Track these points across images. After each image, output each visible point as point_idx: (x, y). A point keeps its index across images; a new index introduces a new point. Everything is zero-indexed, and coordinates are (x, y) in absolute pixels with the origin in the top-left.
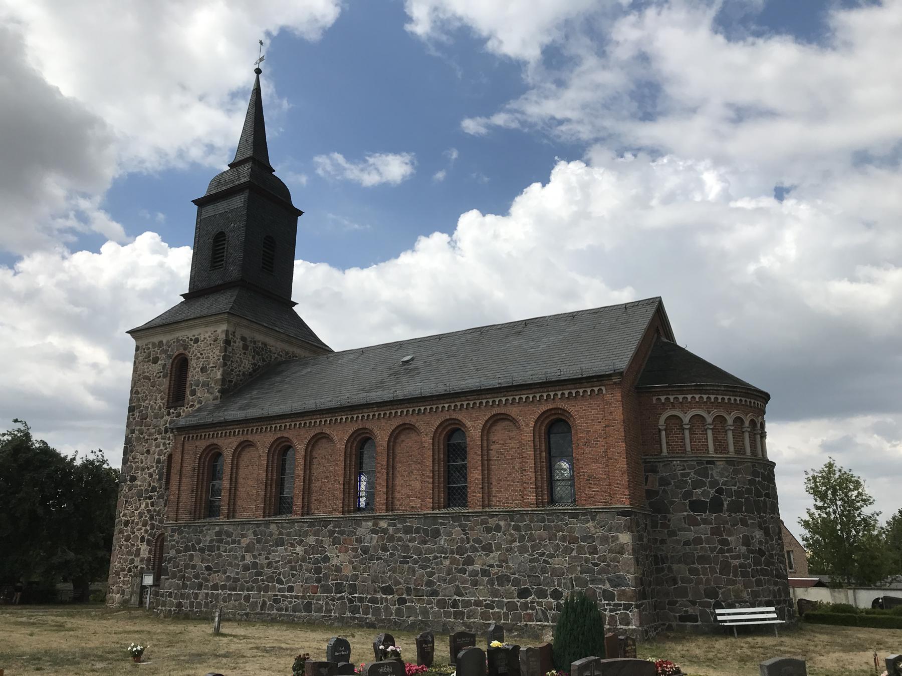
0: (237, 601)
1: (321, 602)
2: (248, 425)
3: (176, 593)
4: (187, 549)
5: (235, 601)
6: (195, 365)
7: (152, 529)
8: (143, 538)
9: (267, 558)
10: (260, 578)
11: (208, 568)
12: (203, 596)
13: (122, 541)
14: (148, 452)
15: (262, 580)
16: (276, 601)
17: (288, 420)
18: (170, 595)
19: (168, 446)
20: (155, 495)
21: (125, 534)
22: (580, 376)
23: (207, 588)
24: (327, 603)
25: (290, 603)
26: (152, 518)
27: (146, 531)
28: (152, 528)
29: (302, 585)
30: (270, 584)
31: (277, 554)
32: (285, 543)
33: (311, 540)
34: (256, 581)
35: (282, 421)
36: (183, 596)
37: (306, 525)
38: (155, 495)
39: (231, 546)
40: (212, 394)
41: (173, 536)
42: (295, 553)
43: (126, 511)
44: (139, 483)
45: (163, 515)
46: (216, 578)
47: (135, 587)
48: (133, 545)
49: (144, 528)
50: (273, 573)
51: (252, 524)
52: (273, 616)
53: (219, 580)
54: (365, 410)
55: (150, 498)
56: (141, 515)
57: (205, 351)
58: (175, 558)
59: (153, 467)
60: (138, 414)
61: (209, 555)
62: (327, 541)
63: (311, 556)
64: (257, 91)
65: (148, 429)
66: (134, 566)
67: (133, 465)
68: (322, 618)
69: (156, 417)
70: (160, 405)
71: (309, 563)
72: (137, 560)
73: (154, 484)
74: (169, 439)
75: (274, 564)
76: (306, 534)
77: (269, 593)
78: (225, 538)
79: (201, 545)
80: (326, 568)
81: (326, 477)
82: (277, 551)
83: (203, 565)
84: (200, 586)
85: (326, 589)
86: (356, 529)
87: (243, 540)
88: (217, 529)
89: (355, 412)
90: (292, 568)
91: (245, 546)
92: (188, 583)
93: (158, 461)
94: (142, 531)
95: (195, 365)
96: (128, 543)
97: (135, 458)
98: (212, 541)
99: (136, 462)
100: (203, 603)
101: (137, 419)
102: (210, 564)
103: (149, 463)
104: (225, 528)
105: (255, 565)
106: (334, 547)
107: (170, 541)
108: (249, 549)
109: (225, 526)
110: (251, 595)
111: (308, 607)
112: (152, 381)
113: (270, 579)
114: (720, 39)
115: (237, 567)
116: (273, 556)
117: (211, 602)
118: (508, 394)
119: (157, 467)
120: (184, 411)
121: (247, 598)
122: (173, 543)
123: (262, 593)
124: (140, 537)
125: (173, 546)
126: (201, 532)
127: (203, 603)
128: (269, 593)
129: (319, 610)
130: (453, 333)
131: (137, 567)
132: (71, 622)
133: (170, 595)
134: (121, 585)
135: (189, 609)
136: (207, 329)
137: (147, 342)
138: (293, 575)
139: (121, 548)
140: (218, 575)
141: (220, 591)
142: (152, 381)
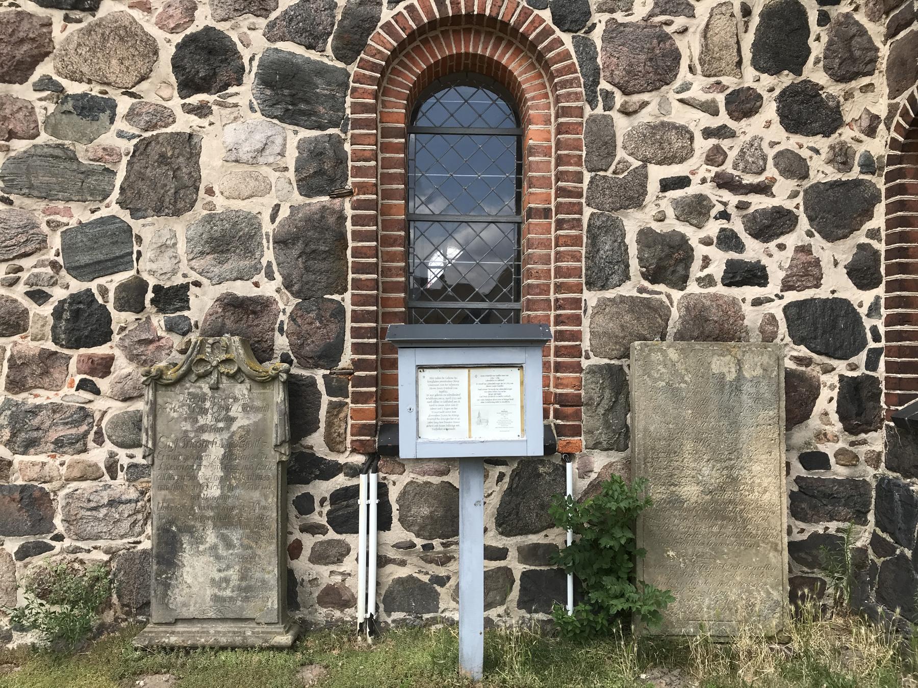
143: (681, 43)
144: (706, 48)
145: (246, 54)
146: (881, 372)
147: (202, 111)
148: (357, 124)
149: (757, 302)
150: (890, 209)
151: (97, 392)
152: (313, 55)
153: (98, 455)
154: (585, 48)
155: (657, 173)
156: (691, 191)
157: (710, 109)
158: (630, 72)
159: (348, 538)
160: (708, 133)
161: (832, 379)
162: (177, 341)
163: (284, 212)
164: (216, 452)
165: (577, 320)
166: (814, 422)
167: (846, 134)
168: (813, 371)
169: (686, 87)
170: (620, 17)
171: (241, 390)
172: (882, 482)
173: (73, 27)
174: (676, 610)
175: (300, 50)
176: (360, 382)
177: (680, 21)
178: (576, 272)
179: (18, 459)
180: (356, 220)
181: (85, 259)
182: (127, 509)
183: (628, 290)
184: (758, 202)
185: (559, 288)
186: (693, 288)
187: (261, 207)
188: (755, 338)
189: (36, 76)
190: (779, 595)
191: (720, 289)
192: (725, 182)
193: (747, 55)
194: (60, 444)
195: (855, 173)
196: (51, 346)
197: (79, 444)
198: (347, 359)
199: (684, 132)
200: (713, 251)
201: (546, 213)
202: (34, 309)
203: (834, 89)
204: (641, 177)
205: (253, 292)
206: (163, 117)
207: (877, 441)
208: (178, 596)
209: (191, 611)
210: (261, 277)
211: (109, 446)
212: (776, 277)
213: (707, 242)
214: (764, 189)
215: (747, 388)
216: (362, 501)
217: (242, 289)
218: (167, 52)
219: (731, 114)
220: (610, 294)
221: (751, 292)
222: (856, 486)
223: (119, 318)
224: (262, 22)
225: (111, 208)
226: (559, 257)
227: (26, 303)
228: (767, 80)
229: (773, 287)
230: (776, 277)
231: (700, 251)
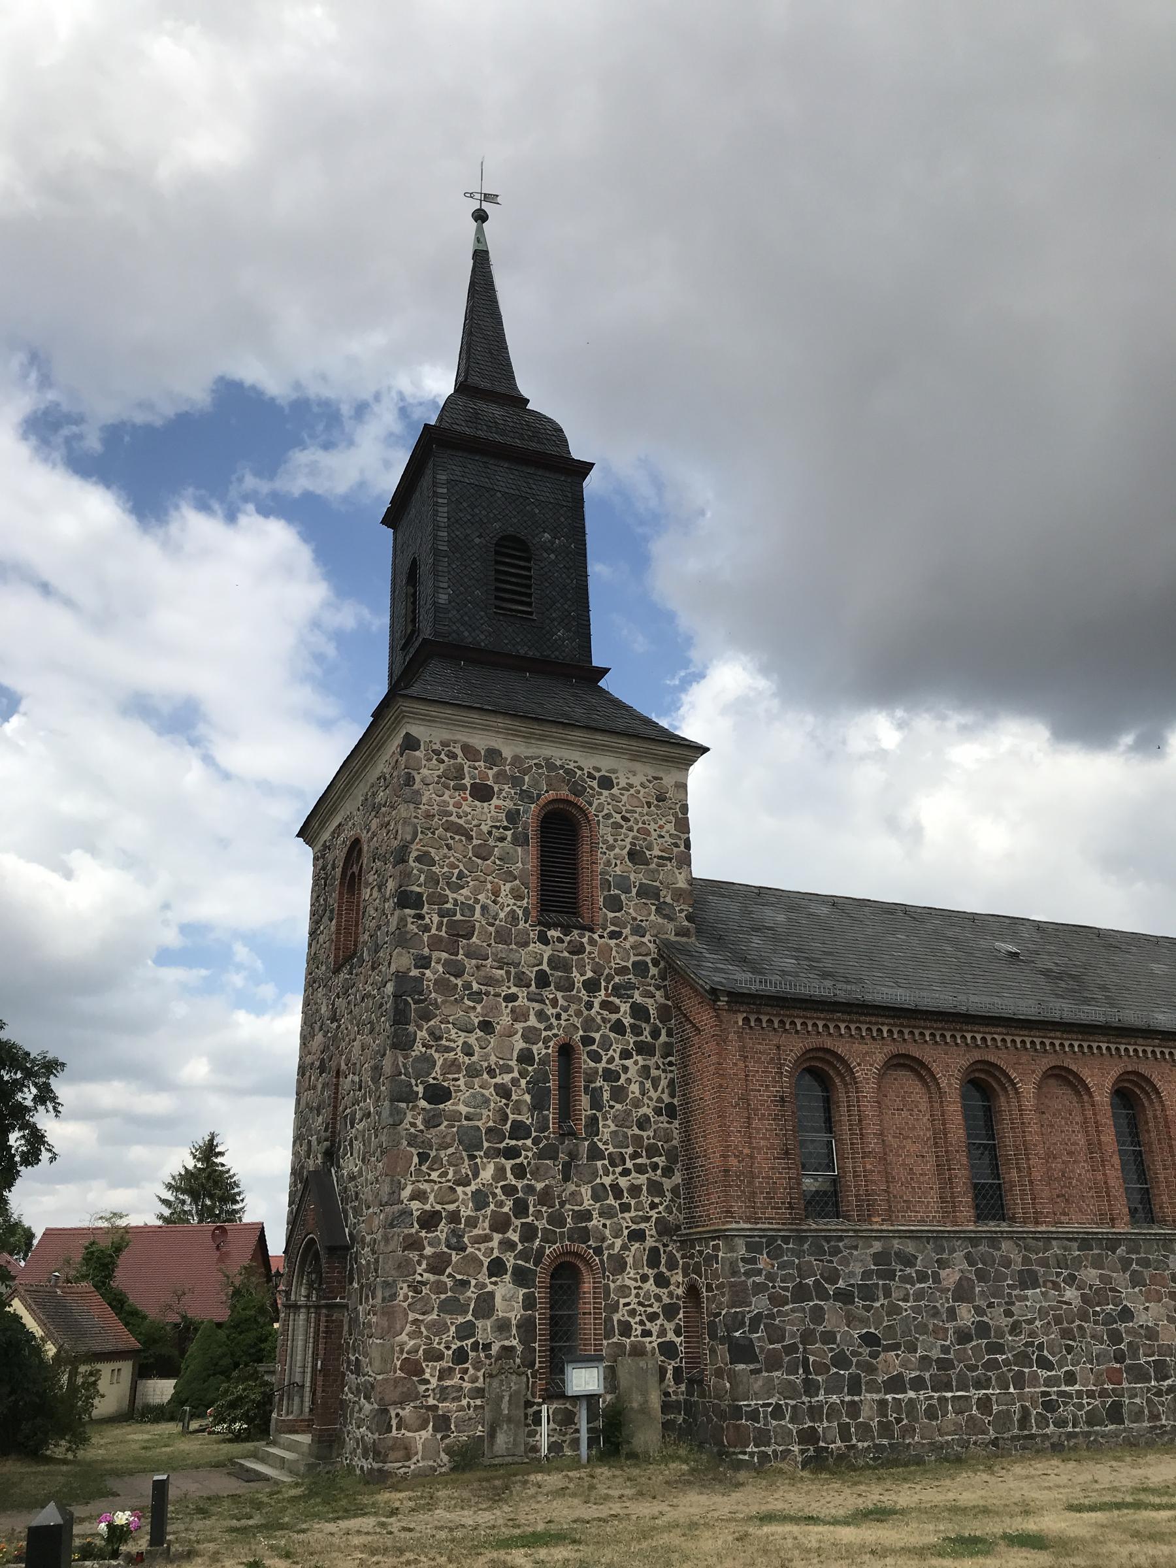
0: (962, 1413)
1: (1137, 1400)
2: (913, 1022)
3: (794, 1407)
4: (801, 1293)
5: (957, 1414)
6: (611, 839)
9: (1008, 1313)
10: (1001, 1357)
12: (871, 1408)
15: (1007, 1362)
16: (1049, 1406)
17: (999, 1030)
18: (778, 1412)
19: (553, 1020)
20: (528, 1149)
21: (428, 1251)
22: (1058, 1020)
23: (873, 1387)
24: (1149, 1401)
25: (1080, 1407)
26: (521, 1208)
27: (508, 1245)
28: (529, 1233)
29: (1091, 1369)
30: (1026, 1370)
31: (1028, 1304)
32: (1041, 1281)
33: (1091, 1275)
34: (992, 1365)
35: (987, 1030)
36: (815, 1412)
37: (1075, 1245)
38: (528, 1149)
39: (918, 1286)
40: (671, 919)
41: (753, 1261)
42: (1066, 1303)
43: (426, 1186)
44: (464, 1110)
45: (562, 1204)
46: (892, 1362)
47: (505, 1405)
48: (465, 1284)
49: (497, 1237)
50: (1027, 1345)
51: (960, 1238)
52: (1055, 1440)
53: (902, 1366)
54: (1140, 1041)
55: (511, 1153)
56: (480, 1200)
57: (636, 815)
58: (772, 1316)
59: (509, 1070)
60: (436, 919)
61: (868, 1309)
62: (1120, 1279)
63: (1098, 1309)
64: (481, 258)
65: (478, 967)
66: (476, 1343)
67: (436, 1056)
68: (1150, 1432)
69: (502, 937)
70: (513, 911)
71: (1096, 1322)
72: (485, 1330)
73: (519, 1118)
74: (554, 1003)
75: (1024, 1325)
76: (1078, 1263)
77: (1027, 1390)
78: (899, 1267)
79: (841, 1284)
80: (1128, 1331)
81: (1070, 1153)
82: (1026, 1298)
83: (855, 1334)
84: (855, 1386)
85: (1139, 1374)
86: (1166, 1257)
87: (943, 1274)
88: (877, 1246)
89: (1123, 1041)
90: (1066, 1334)
91: (952, 1287)
92: (819, 1378)
93: (526, 1058)
94: (495, 1244)
95: (611, 839)
96: (444, 1278)
97: (441, 1038)
98: (867, 1274)
99: (448, 1050)
100: (874, 1424)
101: (433, 931)
102: (872, 1330)
103: (493, 1059)
104: (896, 1244)
105: (983, 1329)
106: (1137, 1289)
107: (748, 1274)
108: (962, 1293)
109: (895, 1242)
110: (994, 1398)
111: (1115, 1413)
112: (475, 842)
114: (23, 450)
115: (941, 1336)
116: (1021, 1308)
117: (899, 1420)
118: (1016, 1032)
119: (523, 1074)
120: (592, 942)
121: (985, 1404)
122: (757, 1279)
123: (1012, 1390)
125: (759, 1288)
126: (836, 1251)
127: (874, 1424)
128: (1027, 1390)
129: (1138, 1416)
130: (869, 900)
131: (487, 1347)
133: (778, 1412)
135: (839, 1443)
136: (637, 766)
137: (446, 735)
138: (1069, 1349)
139: (417, 1291)
140: (897, 1356)
141: (912, 1394)
142: (475, 842)
143: (627, 1259)
144: (634, 1261)
145: (508, 1265)
146: (683, 1365)
147: (495, 1283)
148: (540, 1287)
149: (650, 1343)
150: (684, 1312)
151: (464, 1380)
152: (527, 1265)
153: (464, 1402)
154: (602, 1261)
155: (622, 1301)
156: (631, 1307)
157: (635, 1280)
158: (615, 1270)
159: (538, 1428)
160: (635, 1288)
161: (670, 1367)
162: (488, 1362)
163: (518, 1317)
164: (507, 1398)
165: (602, 1350)
166: (666, 1381)
167: (672, 1287)
168: (666, 1364)
169: (629, 1273)
170: (611, 1252)
171: (514, 1377)
172: (684, 1399)
173: (458, 1257)
174: (635, 1441)
175: (523, 1263)
176: (541, 1374)
177: (627, 1253)
178: (600, 1334)
179: (440, 1405)
180: (539, 1319)
181: (462, 1335)
182: (473, 1421)
183: (615, 1340)
184: (649, 1310)
185: (595, 1339)
186: (633, 1339)
187: (512, 1315)
188: (650, 1355)
189: (447, 1273)
190: (660, 1437)
191: (640, 1339)
192: (640, 1304)
193: (645, 1263)
194: (454, 1399)
195: (675, 1300)
196: (451, 1365)
197: (458, 1399)
198: (537, 1365)
199: (628, 1287)
200: (637, 1326)
201: (590, 1314)
202: (446, 1352)
203: (668, 1274)
204: (618, 1301)
205: (511, 1344)
206: (484, 1286)
207: (683, 1387)
208: (496, 1448)
209: (500, 1453)
210: (512, 1339)
211: (467, 1399)
212: (655, 1334)
213: (636, 1323)
214: (651, 1306)
215: (650, 1371)
216: (542, 1415)
217: (507, 1343)
218: (486, 1264)
219: (603, 1001)
220: (610, 1341)
221: (648, 1339)
222: (678, 1402)
223: (472, 1354)
224: (513, 1254)
225: (469, 1317)
226: (595, 1329)
227: (444, 1350)
228: (651, 1271)
229: (654, 1338)
230: (655, 1334)
231: (635, 1326)
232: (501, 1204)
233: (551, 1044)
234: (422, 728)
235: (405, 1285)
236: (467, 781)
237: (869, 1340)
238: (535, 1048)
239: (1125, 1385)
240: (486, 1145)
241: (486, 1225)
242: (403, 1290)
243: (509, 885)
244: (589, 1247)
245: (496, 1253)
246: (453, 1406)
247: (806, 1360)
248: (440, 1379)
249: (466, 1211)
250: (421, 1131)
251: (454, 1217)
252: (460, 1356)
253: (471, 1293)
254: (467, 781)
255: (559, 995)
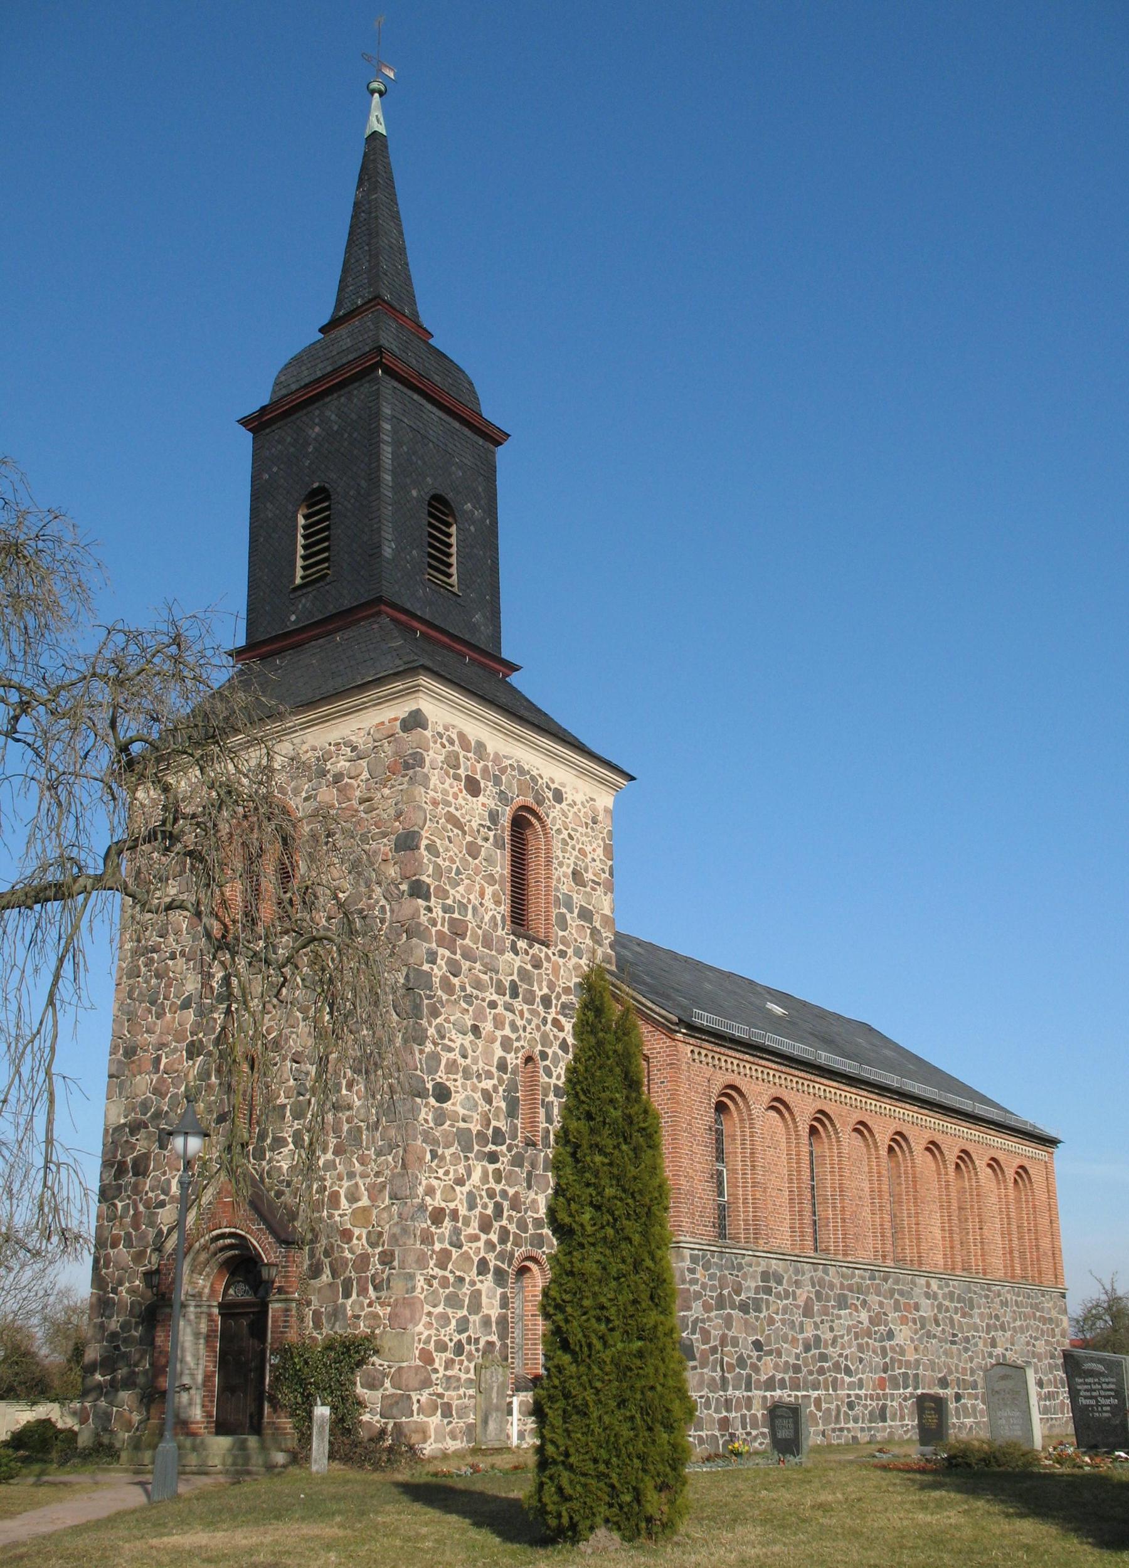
7: (503, 1240)
8: (483, 1263)
10: (826, 1365)
11: (757, 1345)
13: (431, 1265)
14: (476, 1030)
21: (437, 1247)
27: (490, 1245)
28: (504, 1235)
47: (494, 1395)
49: (484, 1237)
55: (493, 1158)
58: (703, 1321)
61: (757, 1318)
79: (743, 1297)
87: (798, 1292)
94: (481, 1244)
113: (837, 1367)
124: (476, 1259)
125: (698, 1296)
131: (477, 1340)
132: (429, 1479)
134: (440, 1390)
138: (861, 1360)
147: (482, 1282)
232: (485, 1206)
233: (520, 1055)
234: (431, 706)
235: (422, 1278)
236: (462, 772)
237: (757, 1345)
238: (508, 1057)
239: (887, 1391)
240: (476, 1148)
241: (476, 1225)
242: (420, 1282)
243: (491, 888)
244: (544, 1253)
245: (482, 1254)
246: (453, 1393)
247: (722, 1359)
248: (446, 1369)
249: (463, 1211)
250: (431, 1128)
251: (454, 1215)
252: (459, 1349)
253: (466, 1290)
254: (462, 772)
255: (526, 1007)
